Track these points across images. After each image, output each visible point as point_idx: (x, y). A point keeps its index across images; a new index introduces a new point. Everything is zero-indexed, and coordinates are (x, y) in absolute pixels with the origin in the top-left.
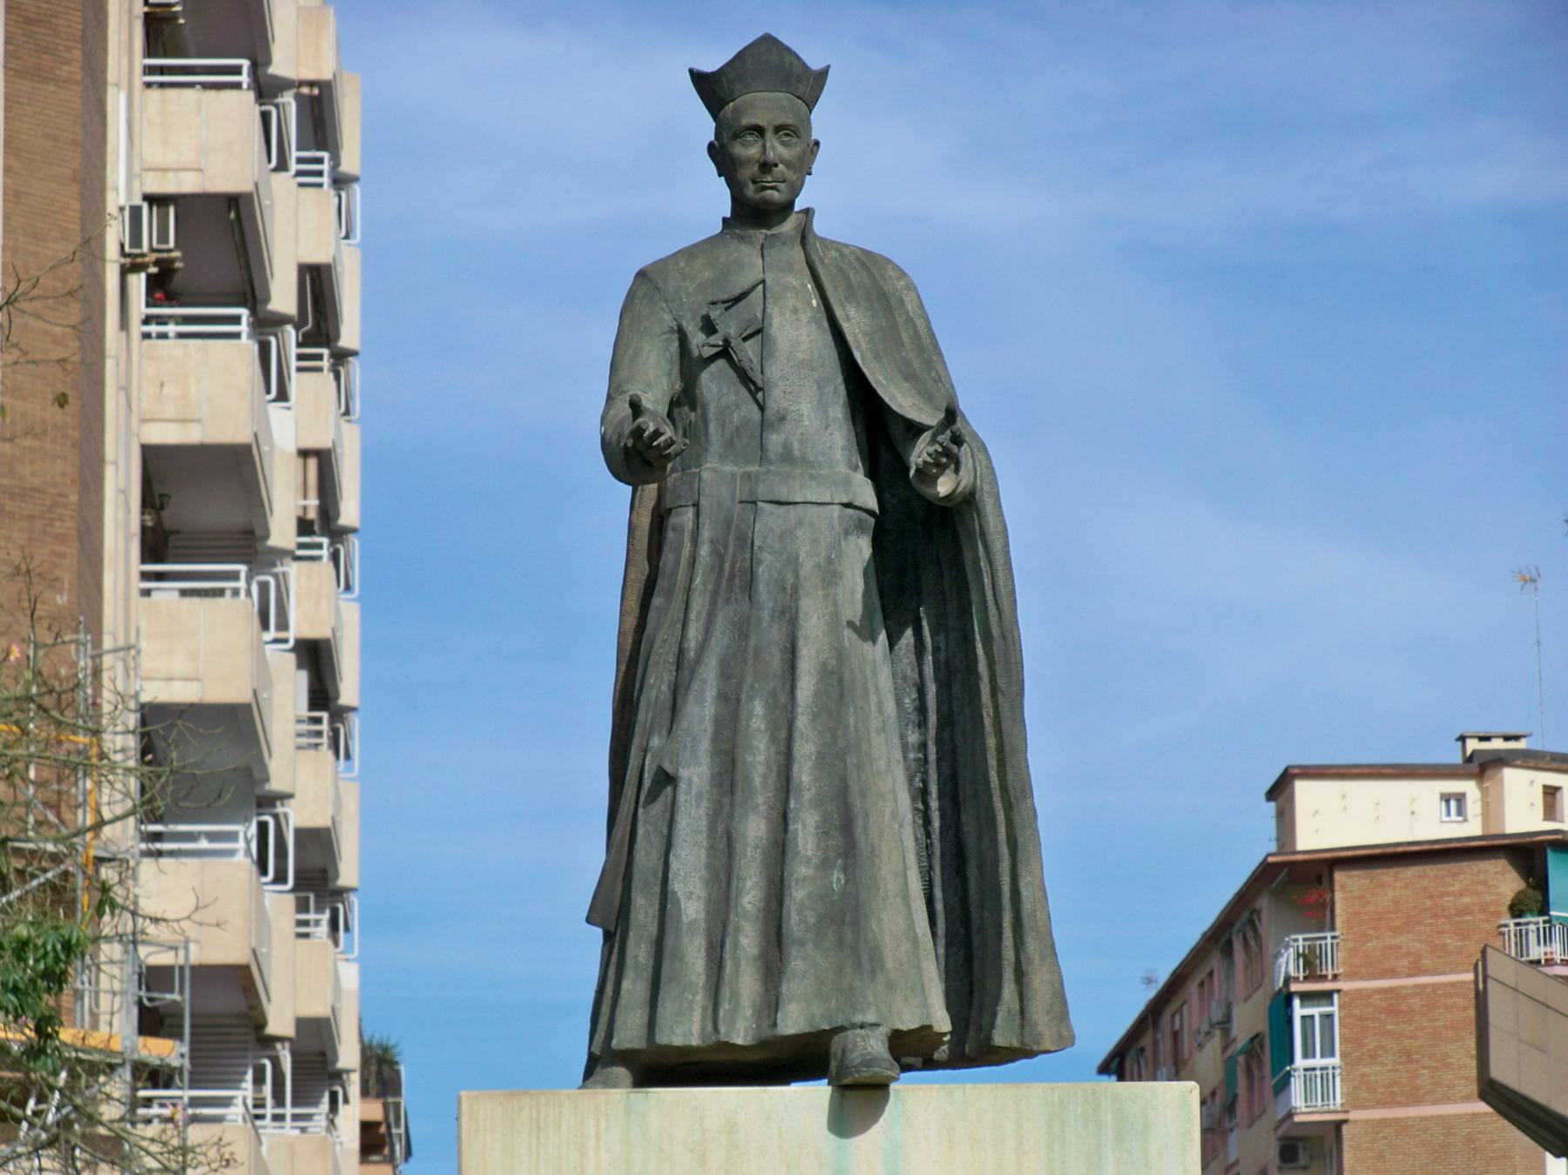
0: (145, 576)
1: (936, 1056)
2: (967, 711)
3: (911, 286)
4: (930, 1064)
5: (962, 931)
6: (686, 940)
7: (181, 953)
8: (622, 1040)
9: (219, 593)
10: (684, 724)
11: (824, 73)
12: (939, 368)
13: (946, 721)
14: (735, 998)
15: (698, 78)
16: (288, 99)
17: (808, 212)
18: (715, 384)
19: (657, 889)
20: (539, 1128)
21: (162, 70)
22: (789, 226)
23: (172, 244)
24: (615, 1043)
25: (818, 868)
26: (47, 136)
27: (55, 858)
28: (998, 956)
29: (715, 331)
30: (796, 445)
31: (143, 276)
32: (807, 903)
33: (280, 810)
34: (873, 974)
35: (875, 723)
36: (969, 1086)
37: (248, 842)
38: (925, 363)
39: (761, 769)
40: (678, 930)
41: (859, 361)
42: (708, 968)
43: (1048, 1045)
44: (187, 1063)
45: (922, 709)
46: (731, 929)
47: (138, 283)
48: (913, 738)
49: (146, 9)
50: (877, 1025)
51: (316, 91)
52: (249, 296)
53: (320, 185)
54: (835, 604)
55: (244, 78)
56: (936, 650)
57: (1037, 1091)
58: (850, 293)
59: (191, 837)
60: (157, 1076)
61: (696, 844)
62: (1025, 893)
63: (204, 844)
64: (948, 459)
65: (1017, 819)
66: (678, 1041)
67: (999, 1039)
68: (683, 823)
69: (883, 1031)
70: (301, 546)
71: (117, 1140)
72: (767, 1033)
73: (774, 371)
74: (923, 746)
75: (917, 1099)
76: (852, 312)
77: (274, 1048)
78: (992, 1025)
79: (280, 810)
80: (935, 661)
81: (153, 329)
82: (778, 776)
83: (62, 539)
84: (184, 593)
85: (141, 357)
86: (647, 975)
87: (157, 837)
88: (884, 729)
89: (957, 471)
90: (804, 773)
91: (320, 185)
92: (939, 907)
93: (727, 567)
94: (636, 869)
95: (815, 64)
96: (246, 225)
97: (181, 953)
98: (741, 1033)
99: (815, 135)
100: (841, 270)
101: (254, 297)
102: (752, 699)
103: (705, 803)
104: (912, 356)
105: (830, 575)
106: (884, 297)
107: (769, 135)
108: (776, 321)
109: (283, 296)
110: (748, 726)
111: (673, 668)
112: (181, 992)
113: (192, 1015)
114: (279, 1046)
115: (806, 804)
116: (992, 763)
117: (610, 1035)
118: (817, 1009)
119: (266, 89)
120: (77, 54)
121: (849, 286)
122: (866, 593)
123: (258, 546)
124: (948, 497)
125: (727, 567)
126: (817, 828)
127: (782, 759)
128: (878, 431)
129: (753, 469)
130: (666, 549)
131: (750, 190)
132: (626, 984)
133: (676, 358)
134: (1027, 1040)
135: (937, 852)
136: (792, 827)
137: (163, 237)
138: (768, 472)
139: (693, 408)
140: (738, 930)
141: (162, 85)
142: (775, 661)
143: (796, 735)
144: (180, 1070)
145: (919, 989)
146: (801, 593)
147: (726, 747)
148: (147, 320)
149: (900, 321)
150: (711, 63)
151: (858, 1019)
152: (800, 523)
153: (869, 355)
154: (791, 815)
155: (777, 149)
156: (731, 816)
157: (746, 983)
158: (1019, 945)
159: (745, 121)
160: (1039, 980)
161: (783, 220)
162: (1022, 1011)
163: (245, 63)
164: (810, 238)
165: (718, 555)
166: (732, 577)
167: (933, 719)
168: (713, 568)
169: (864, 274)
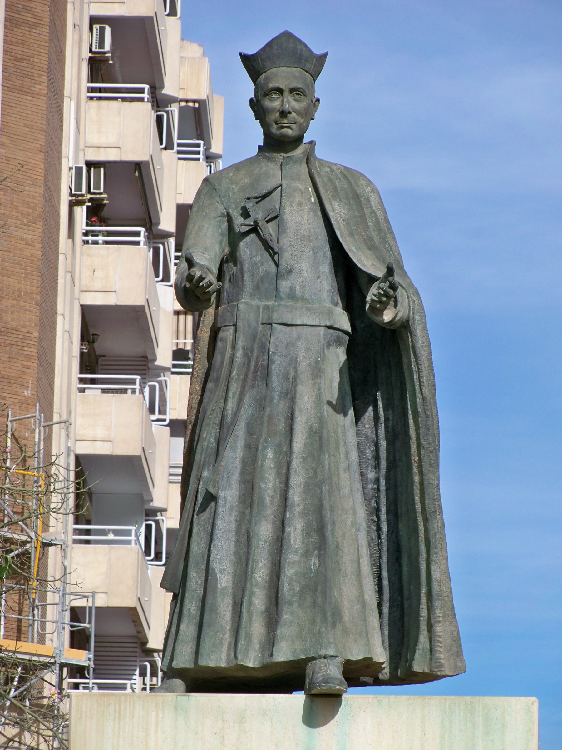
0: (82, 381)
1: (381, 676)
2: (404, 459)
3: (375, 190)
4: (378, 682)
5: (399, 598)
6: (219, 599)
7: (90, 600)
8: (178, 664)
9: (124, 391)
10: (223, 463)
11: (325, 55)
12: (391, 242)
13: (392, 465)
14: (249, 637)
15: (246, 59)
16: (174, 109)
17: (312, 143)
18: (248, 248)
19: (204, 567)
20: (120, 716)
21: (100, 90)
22: (299, 152)
23: (102, 190)
24: (175, 664)
25: (302, 556)
26: (25, 125)
27: (24, 543)
28: (418, 615)
29: (250, 216)
30: (298, 289)
31: (84, 207)
32: (294, 578)
33: (159, 517)
34: (334, 625)
35: (343, 465)
36: (393, 697)
37: (137, 536)
38: (381, 237)
39: (270, 493)
40: (216, 592)
41: (339, 236)
42: (233, 618)
43: (447, 672)
44: (92, 666)
45: (377, 457)
46: (247, 593)
47: (81, 212)
48: (371, 475)
49: (90, 55)
50: (336, 657)
51: (197, 105)
52: (148, 221)
53: (198, 159)
54: (319, 389)
55: (146, 96)
56: (387, 420)
57: (435, 700)
58: (336, 194)
59: (104, 533)
60: (78, 671)
61: (228, 539)
62: (435, 575)
63: (111, 537)
64: (389, 298)
65: (431, 528)
66: (212, 664)
67: (417, 667)
68: (220, 525)
69: (339, 660)
70: (174, 366)
71: (51, 707)
72: (267, 660)
73: (285, 242)
74: (377, 481)
75: (360, 706)
76: (336, 205)
77: (153, 657)
78: (413, 659)
79: (159, 517)
80: (386, 427)
81: (90, 238)
82: (280, 497)
83: (28, 358)
84: (104, 391)
85: (82, 254)
86: (196, 621)
87: (88, 532)
88: (349, 469)
89: (395, 306)
90: (296, 496)
91: (198, 159)
92: (385, 582)
93: (253, 364)
94: (191, 554)
95: (318, 51)
96: (145, 180)
97: (90, 600)
98: (251, 660)
99: (317, 95)
100: (331, 180)
101: (151, 221)
102: (266, 448)
103: (234, 513)
104: (374, 234)
105: (317, 372)
106: (357, 196)
107: (286, 94)
108: (288, 210)
109: (167, 222)
110: (262, 465)
111: (218, 427)
112: (90, 623)
113: (95, 636)
114: (155, 655)
115: (297, 515)
116: (417, 491)
117: (172, 660)
118: (298, 646)
119: (159, 102)
120: (45, 79)
121: (335, 189)
122: (341, 384)
123: (150, 365)
124: (390, 323)
125: (253, 364)
126: (303, 530)
127: (283, 486)
128: (350, 280)
129: (270, 303)
130: (217, 352)
131: (274, 129)
132: (183, 627)
133: (226, 232)
134: (433, 669)
135: (385, 547)
136: (287, 530)
137: (97, 187)
138: (279, 305)
139: (235, 264)
140: (252, 594)
141: (100, 98)
142: (281, 424)
143: (292, 471)
144: (88, 668)
145: (364, 634)
146: (298, 381)
147: (249, 477)
148: (86, 234)
149: (367, 212)
150: (252, 48)
151: (323, 652)
152: (299, 338)
153: (346, 233)
154: (287, 522)
155: (291, 103)
156: (250, 522)
157: (257, 628)
158: (430, 609)
159: (271, 85)
160: (443, 631)
161: (296, 148)
162: (431, 650)
163: (146, 87)
164: (312, 159)
165: (247, 357)
166: (256, 371)
167: (383, 463)
168: (244, 364)
169: (345, 182)
